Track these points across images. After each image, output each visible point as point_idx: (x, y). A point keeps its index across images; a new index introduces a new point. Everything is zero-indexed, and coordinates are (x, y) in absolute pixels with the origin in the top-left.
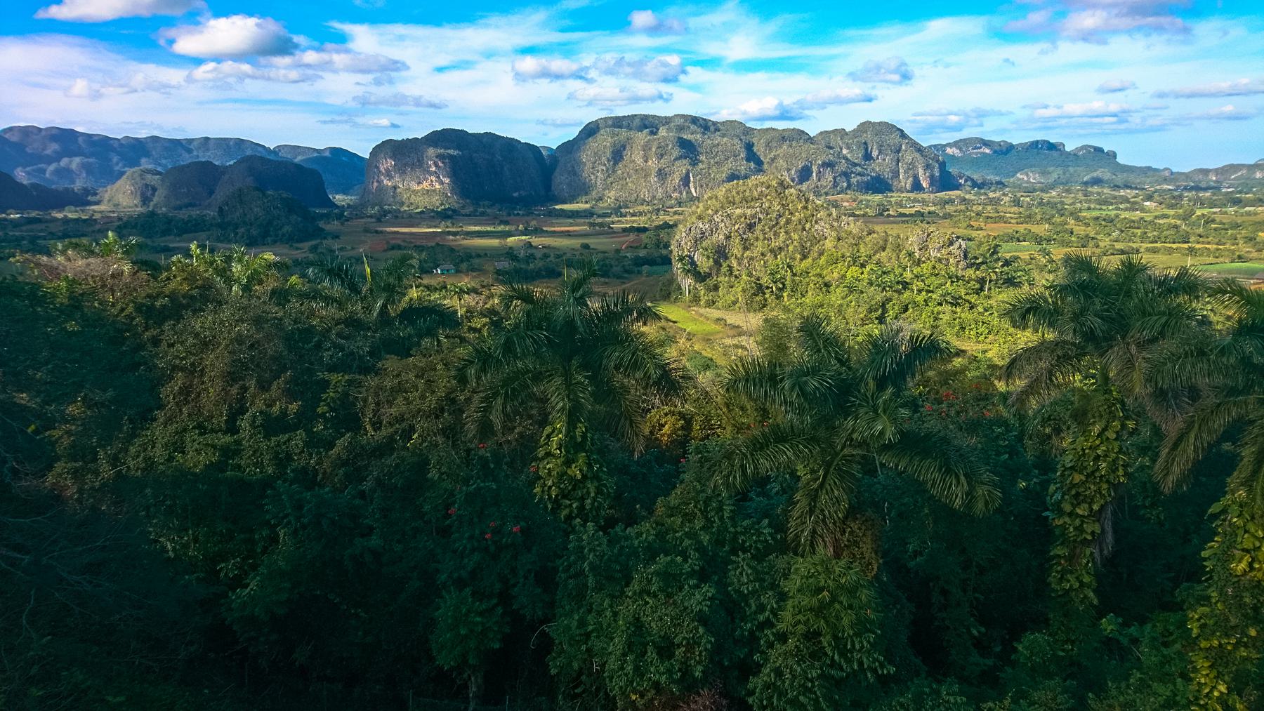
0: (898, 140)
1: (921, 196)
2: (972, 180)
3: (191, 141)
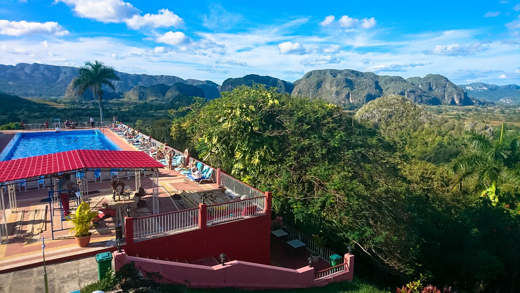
0: (445, 82)
1: (455, 107)
2: (479, 101)
3: (156, 76)
